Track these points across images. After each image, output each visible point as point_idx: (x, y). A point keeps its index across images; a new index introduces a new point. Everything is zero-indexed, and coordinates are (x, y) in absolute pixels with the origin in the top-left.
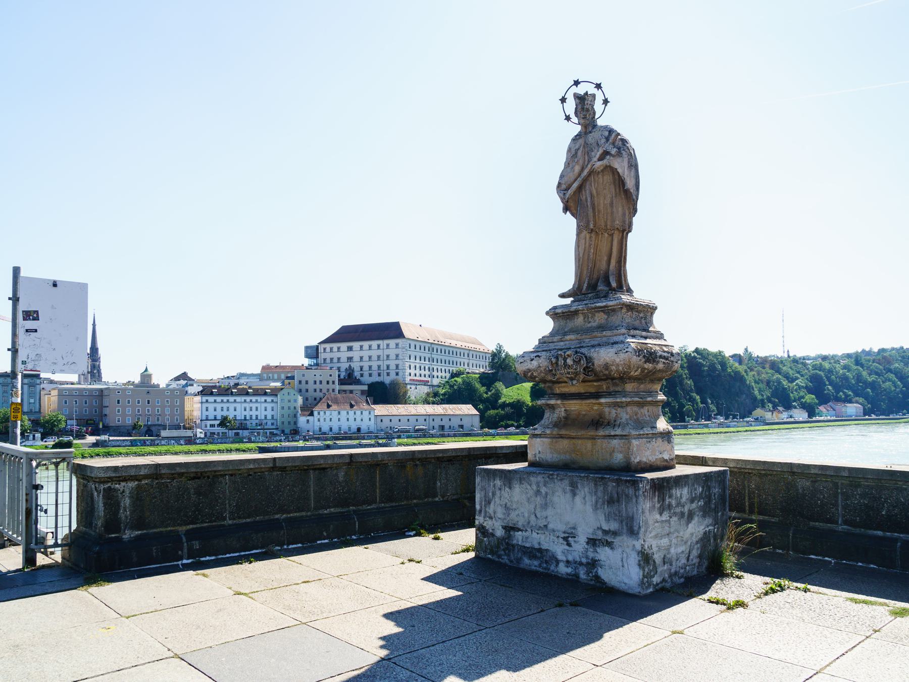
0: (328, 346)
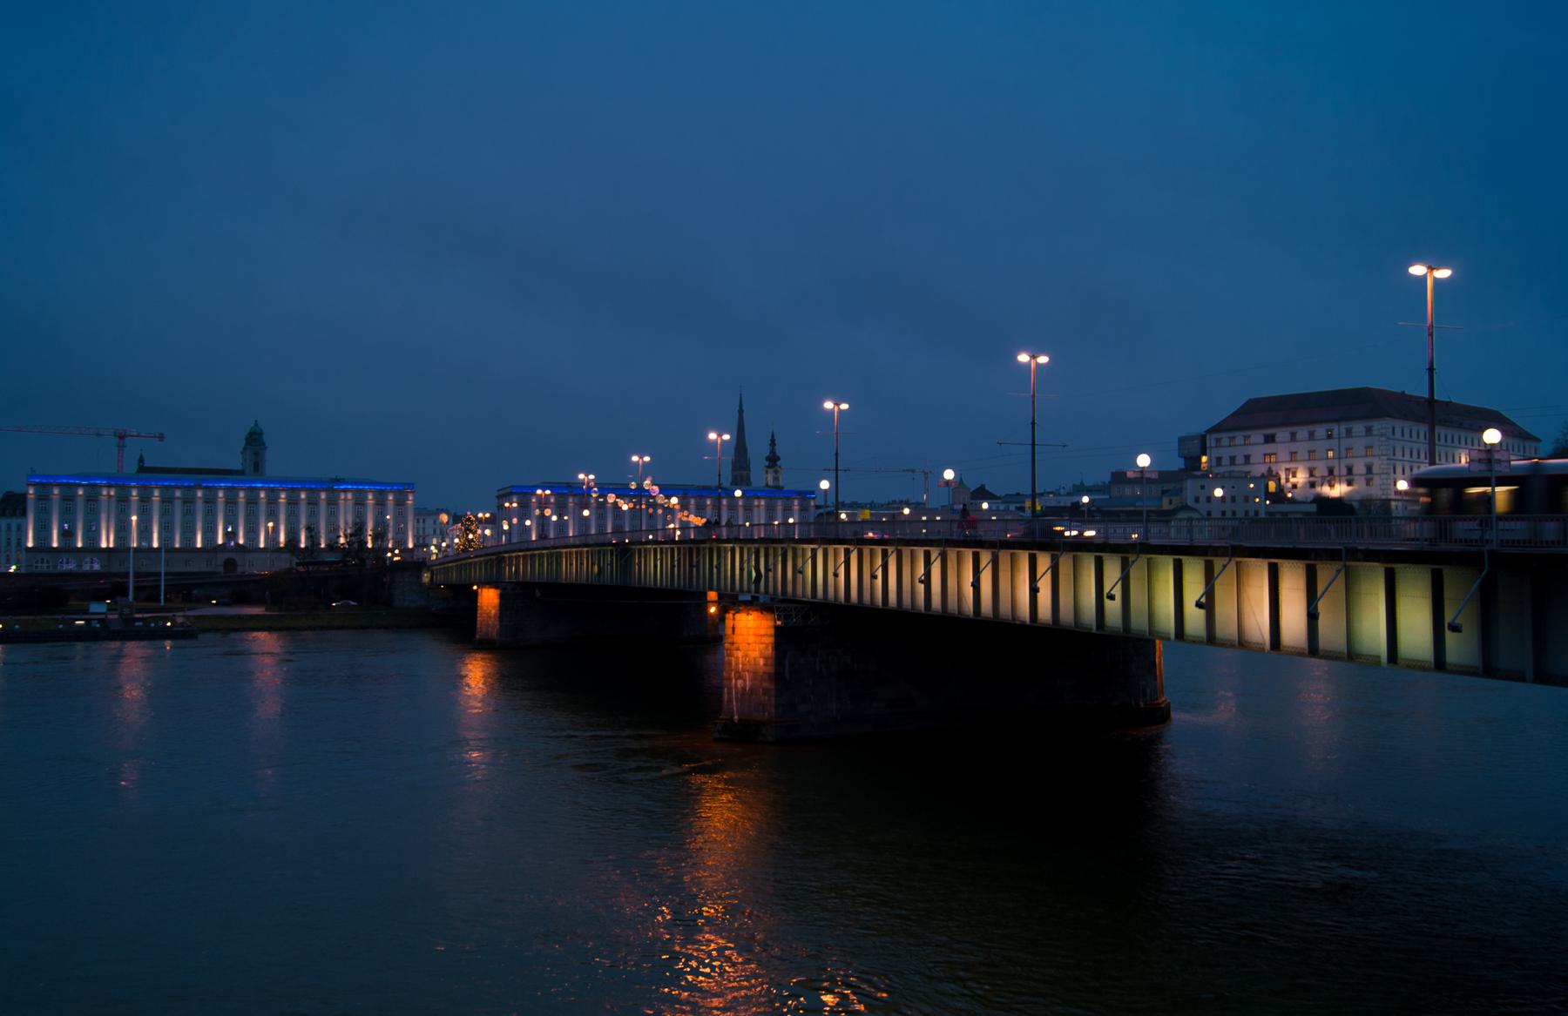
0: (1225, 437)
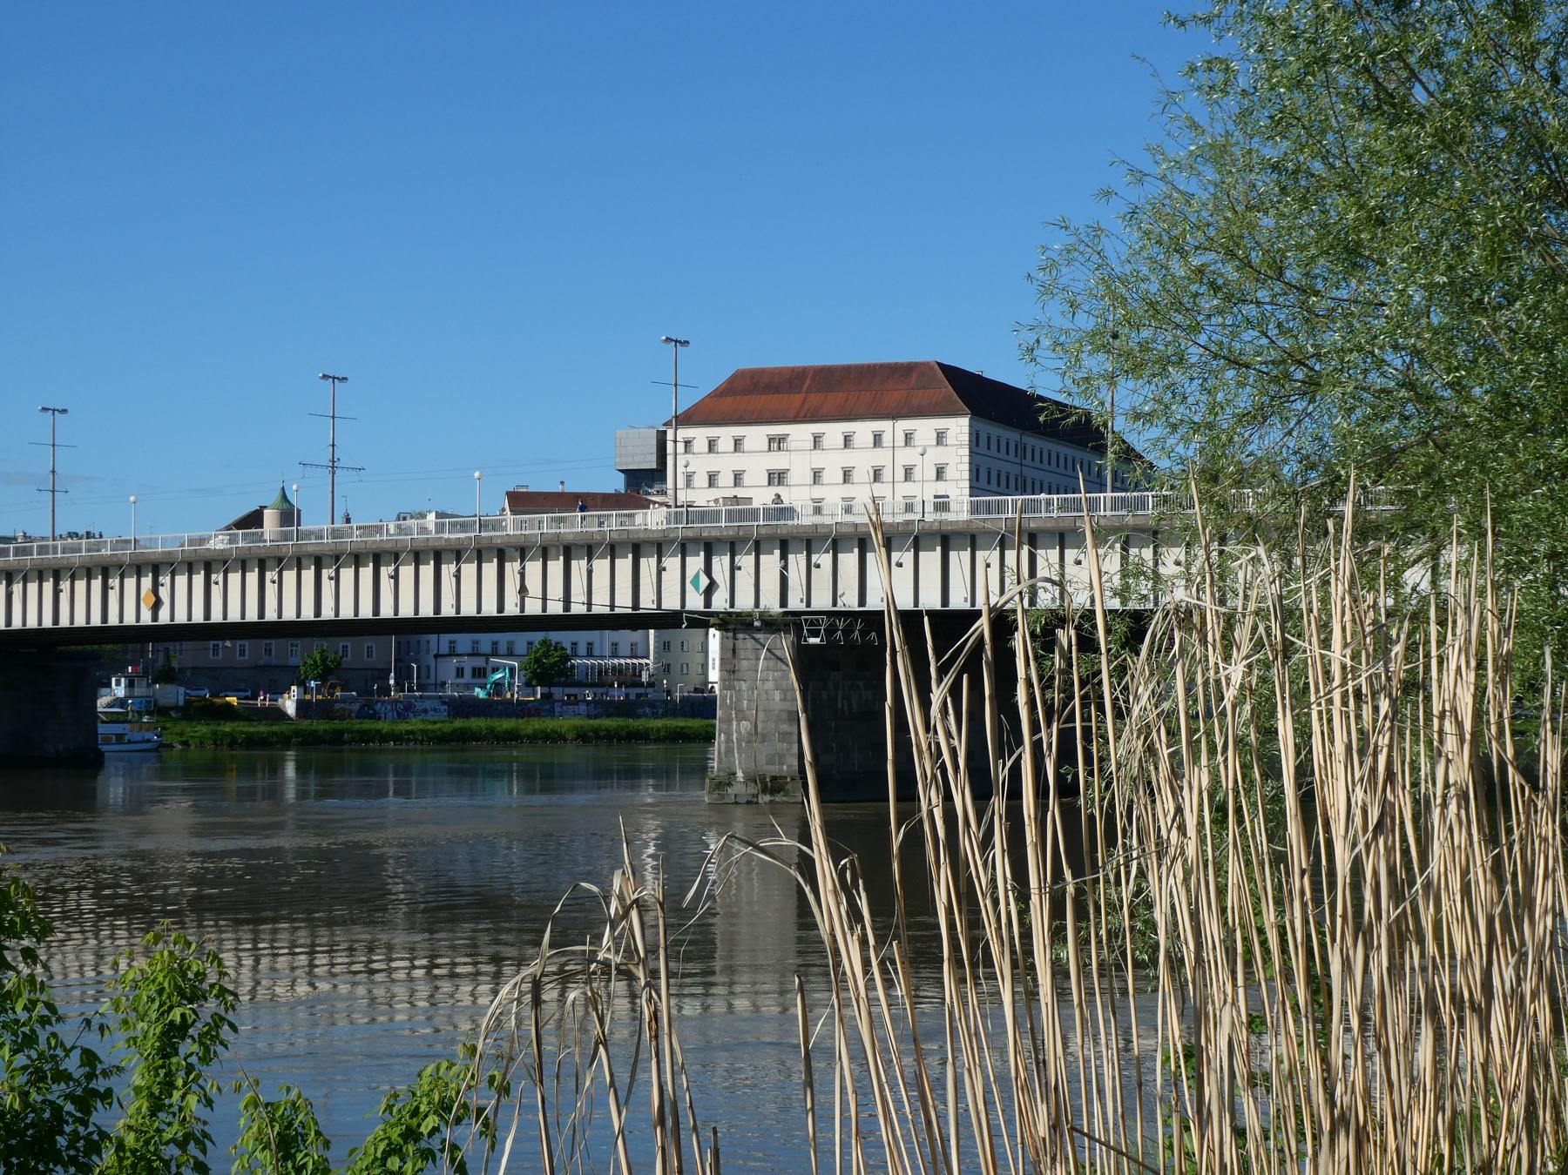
0: (700, 435)
